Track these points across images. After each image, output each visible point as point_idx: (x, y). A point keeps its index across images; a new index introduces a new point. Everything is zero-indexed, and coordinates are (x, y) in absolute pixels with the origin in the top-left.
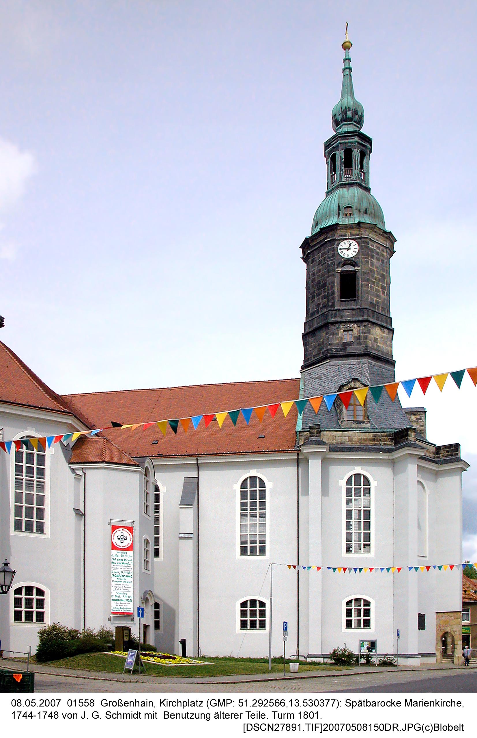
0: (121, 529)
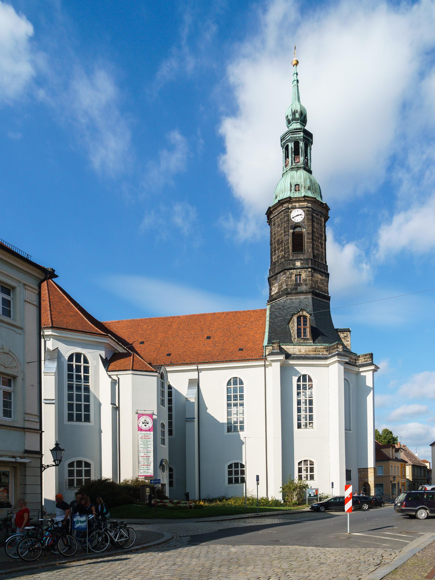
0: (145, 416)
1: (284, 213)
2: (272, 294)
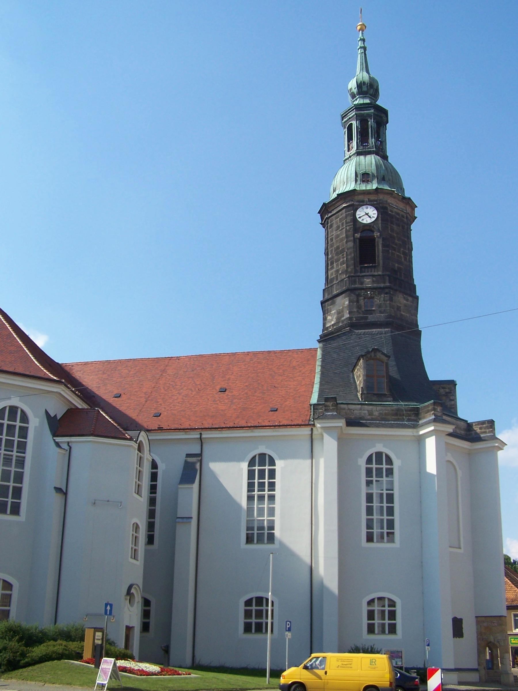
1: (346, 212)
2: (326, 326)
